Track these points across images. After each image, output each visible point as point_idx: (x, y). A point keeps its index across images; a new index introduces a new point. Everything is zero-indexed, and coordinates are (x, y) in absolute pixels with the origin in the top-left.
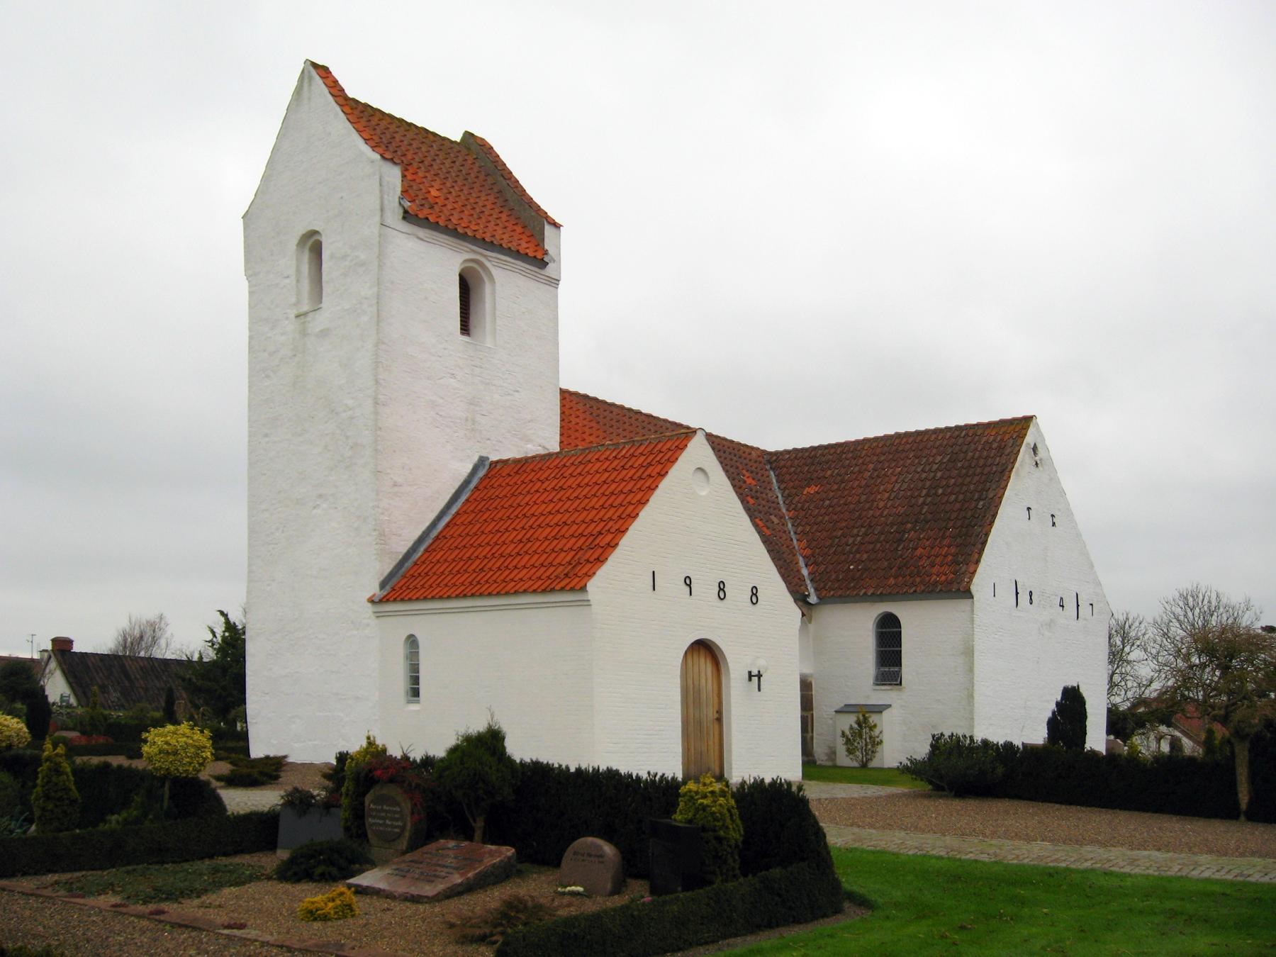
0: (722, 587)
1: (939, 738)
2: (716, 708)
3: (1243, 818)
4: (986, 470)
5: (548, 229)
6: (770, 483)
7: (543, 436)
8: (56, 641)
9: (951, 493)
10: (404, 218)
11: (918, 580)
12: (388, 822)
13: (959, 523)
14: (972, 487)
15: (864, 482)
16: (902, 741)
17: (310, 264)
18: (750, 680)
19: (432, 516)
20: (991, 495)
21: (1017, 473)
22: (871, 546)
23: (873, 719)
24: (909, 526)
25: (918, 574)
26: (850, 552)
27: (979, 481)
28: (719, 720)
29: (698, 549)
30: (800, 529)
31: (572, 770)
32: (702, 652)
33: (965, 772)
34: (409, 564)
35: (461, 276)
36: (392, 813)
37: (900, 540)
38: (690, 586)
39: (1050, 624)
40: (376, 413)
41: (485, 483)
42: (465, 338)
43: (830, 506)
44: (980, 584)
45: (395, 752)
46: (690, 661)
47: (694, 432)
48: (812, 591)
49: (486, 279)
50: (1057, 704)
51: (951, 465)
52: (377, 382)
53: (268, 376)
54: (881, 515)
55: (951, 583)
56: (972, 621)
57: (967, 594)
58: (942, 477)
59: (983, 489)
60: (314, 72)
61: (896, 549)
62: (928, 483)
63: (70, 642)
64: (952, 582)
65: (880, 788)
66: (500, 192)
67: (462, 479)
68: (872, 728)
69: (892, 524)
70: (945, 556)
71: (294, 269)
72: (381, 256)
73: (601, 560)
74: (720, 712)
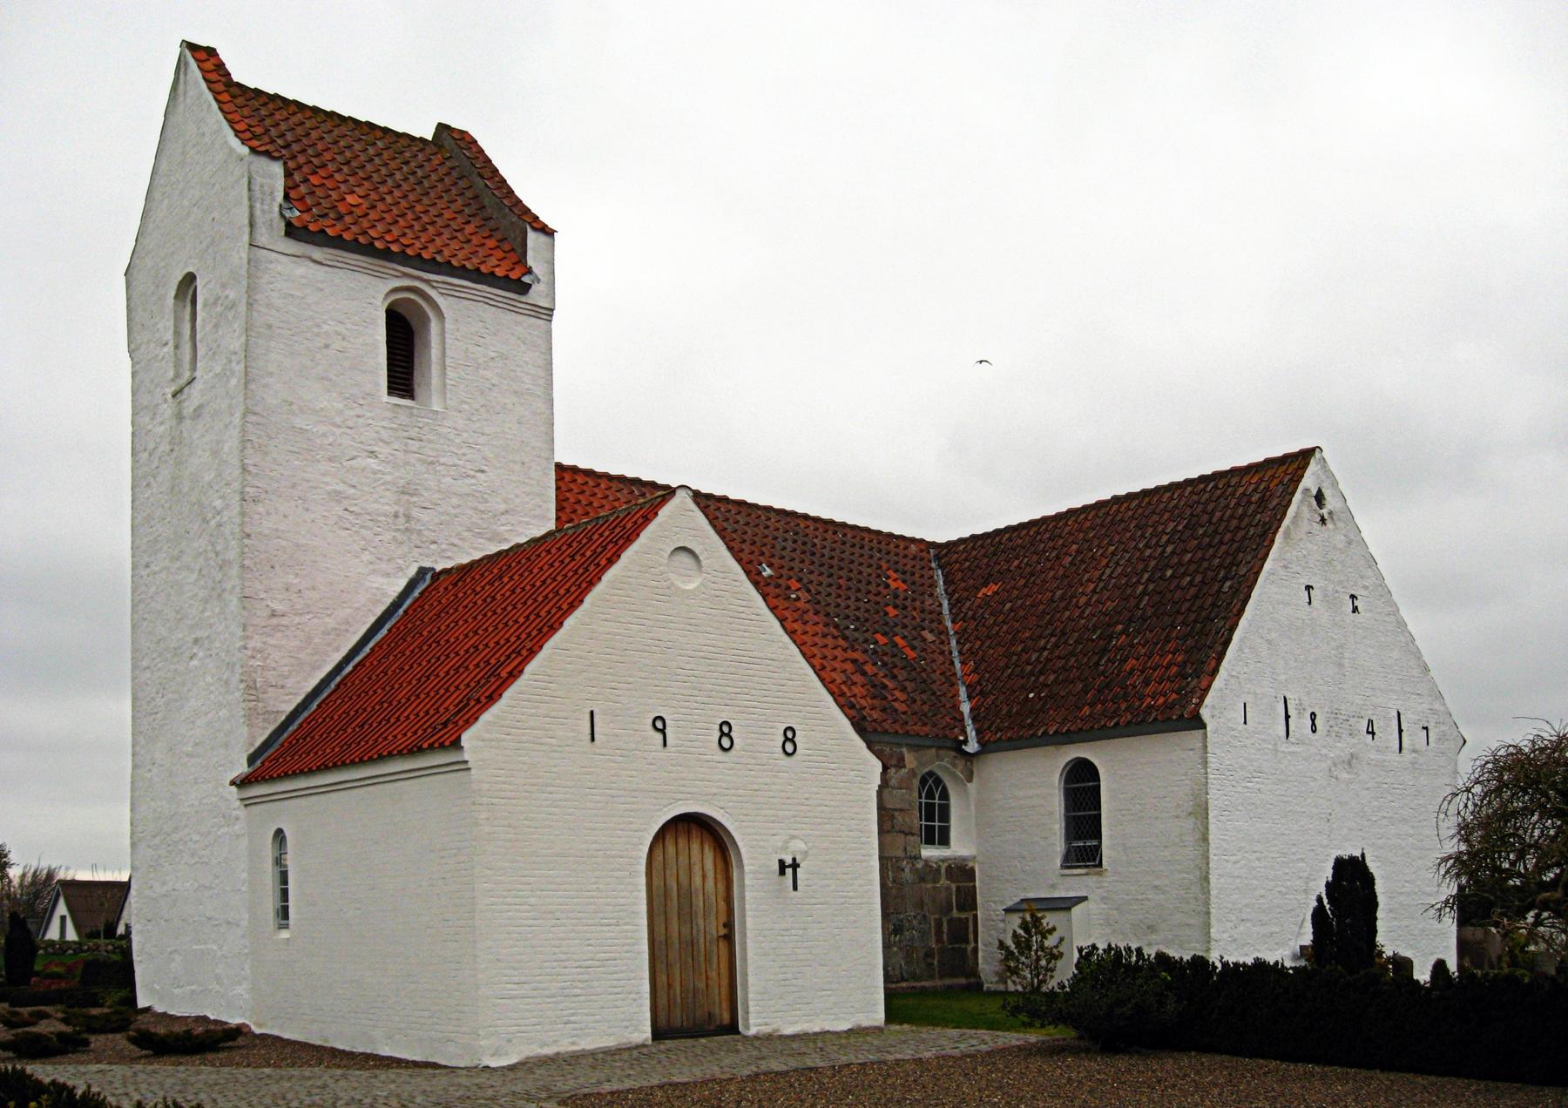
1: (1090, 954)
2: (723, 919)
5: (532, 237)
6: (933, 585)
9: (1184, 574)
11: (1123, 706)
13: (1192, 617)
14: (1216, 561)
15: (1061, 572)
18: (782, 872)
20: (1243, 571)
21: (1287, 535)
22: (1061, 663)
23: (1049, 920)
25: (1125, 698)
26: (1031, 673)
27: (1227, 552)
28: (729, 938)
32: (695, 832)
37: (1105, 650)
38: (663, 731)
39: (1351, 761)
40: (243, 514)
44: (1220, 703)
47: (669, 492)
49: (431, 314)
51: (1188, 533)
52: (244, 469)
55: (1171, 707)
56: (1205, 763)
57: (1198, 723)
58: (1173, 553)
59: (1232, 564)
61: (1097, 664)
62: (1153, 563)
65: (984, 1034)
66: (476, 197)
67: (388, 601)
69: (1095, 628)
70: (1167, 668)
71: (171, 332)
72: (251, 289)
74: (729, 925)
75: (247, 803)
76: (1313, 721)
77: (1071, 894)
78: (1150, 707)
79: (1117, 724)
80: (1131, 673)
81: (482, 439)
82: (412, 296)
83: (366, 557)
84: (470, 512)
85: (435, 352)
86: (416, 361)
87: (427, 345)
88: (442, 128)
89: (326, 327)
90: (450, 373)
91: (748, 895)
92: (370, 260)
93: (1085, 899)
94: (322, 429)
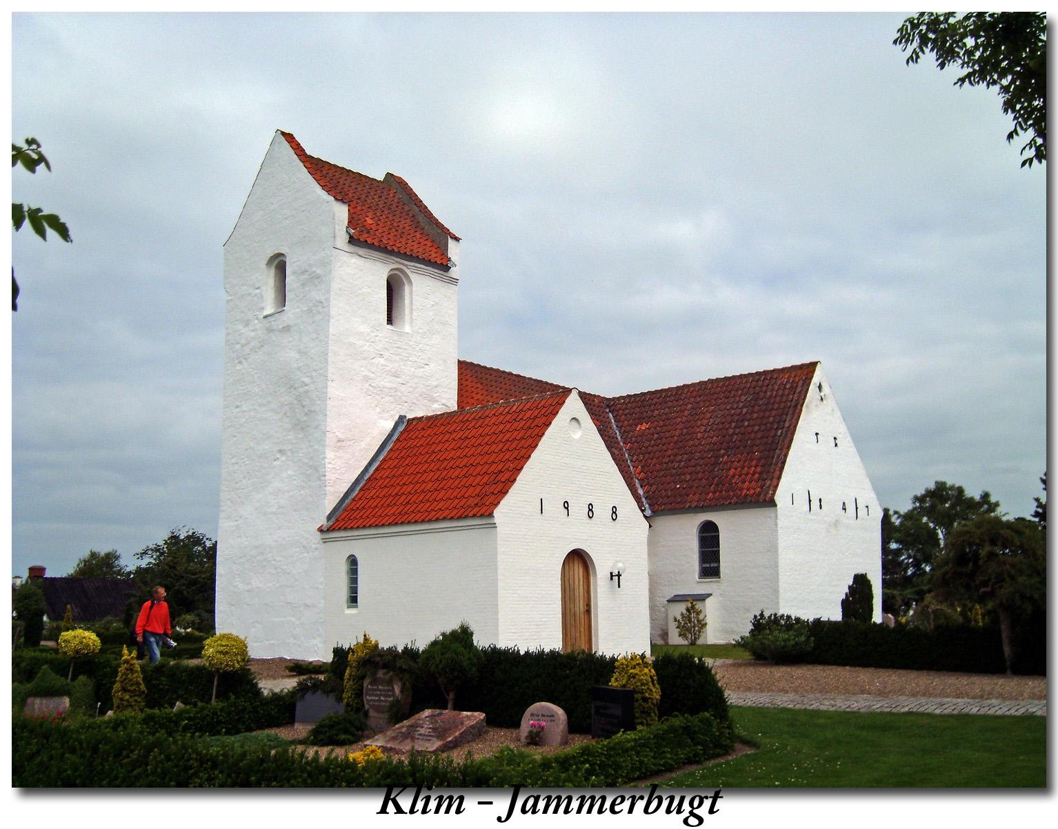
0: (590, 508)
3: (1009, 672)
4: (782, 405)
5: (451, 243)
6: (610, 422)
7: (446, 399)
8: (32, 570)
10: (349, 242)
12: (382, 698)
14: (771, 419)
16: (723, 623)
17: (275, 277)
18: (612, 579)
19: (365, 463)
21: (807, 406)
23: (699, 606)
24: (723, 451)
28: (588, 612)
29: (570, 483)
30: (635, 457)
31: (522, 653)
33: (778, 643)
34: (347, 501)
35: (387, 281)
36: (383, 693)
37: (715, 464)
38: (567, 508)
39: (836, 524)
41: (404, 436)
42: (389, 327)
43: (658, 438)
44: (781, 496)
45: (384, 645)
46: (567, 567)
47: (569, 391)
48: (647, 506)
50: (849, 587)
53: (240, 362)
54: (700, 444)
56: (776, 525)
57: (772, 503)
60: (283, 139)
63: (42, 570)
64: (761, 496)
66: (413, 216)
68: (698, 613)
73: (504, 492)
74: (588, 605)
75: (325, 541)
76: (821, 505)
77: (703, 592)
78: (746, 495)
79: (730, 503)
80: (734, 476)
81: (428, 348)
82: (398, 273)
83: (378, 410)
84: (422, 386)
85: (407, 301)
86: (394, 303)
87: (402, 298)
88: (389, 175)
89: (364, 290)
90: (415, 313)
91: (599, 590)
92: (381, 254)
93: (711, 595)
94: (361, 343)
